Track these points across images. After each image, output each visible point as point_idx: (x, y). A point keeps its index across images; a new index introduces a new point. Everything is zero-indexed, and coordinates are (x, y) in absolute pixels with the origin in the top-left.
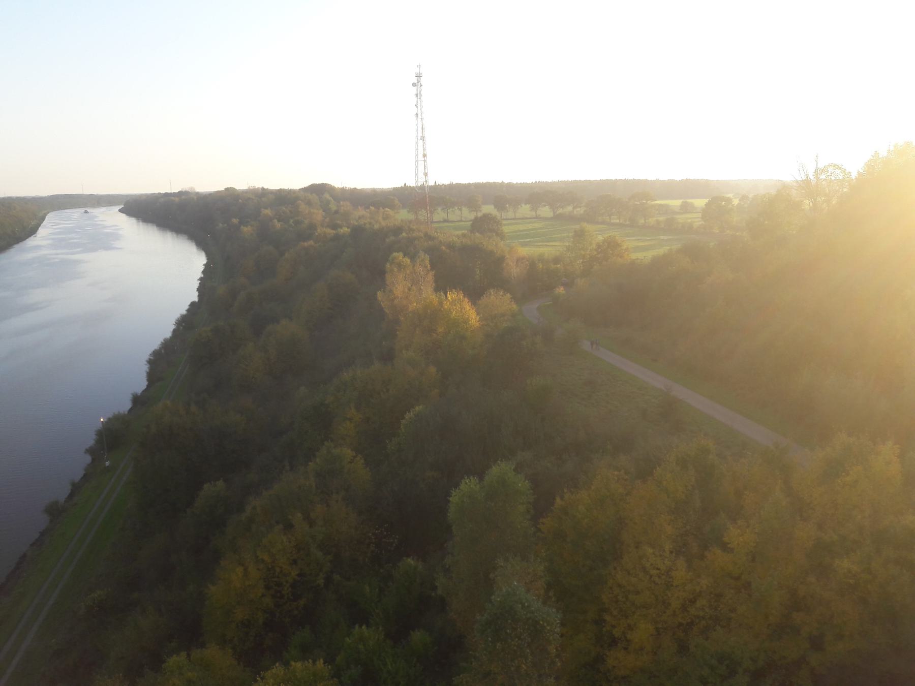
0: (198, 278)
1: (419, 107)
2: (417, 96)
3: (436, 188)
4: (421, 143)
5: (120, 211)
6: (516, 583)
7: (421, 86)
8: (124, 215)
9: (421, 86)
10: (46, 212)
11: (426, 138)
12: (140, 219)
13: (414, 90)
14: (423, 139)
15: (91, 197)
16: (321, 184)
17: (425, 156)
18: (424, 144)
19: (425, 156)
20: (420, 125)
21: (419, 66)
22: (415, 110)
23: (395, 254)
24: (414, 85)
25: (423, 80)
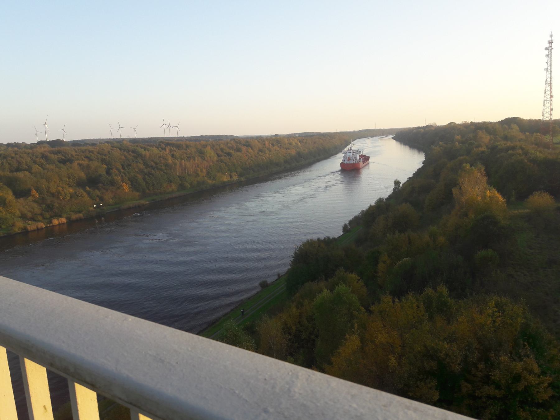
0: (408, 178)
1: (549, 64)
2: (548, 56)
3: (555, 120)
4: (549, 88)
5: (393, 138)
6: (345, 298)
7: (552, 49)
8: (394, 141)
9: (552, 49)
10: (36, 145)
11: (553, 85)
12: (402, 143)
13: (547, 52)
14: (551, 85)
15: (380, 130)
16: (513, 117)
17: (552, 96)
18: (551, 88)
19: (552, 96)
20: (549, 76)
21: (551, 36)
22: (545, 66)
23: (464, 165)
24: (546, 49)
25: (553, 45)
